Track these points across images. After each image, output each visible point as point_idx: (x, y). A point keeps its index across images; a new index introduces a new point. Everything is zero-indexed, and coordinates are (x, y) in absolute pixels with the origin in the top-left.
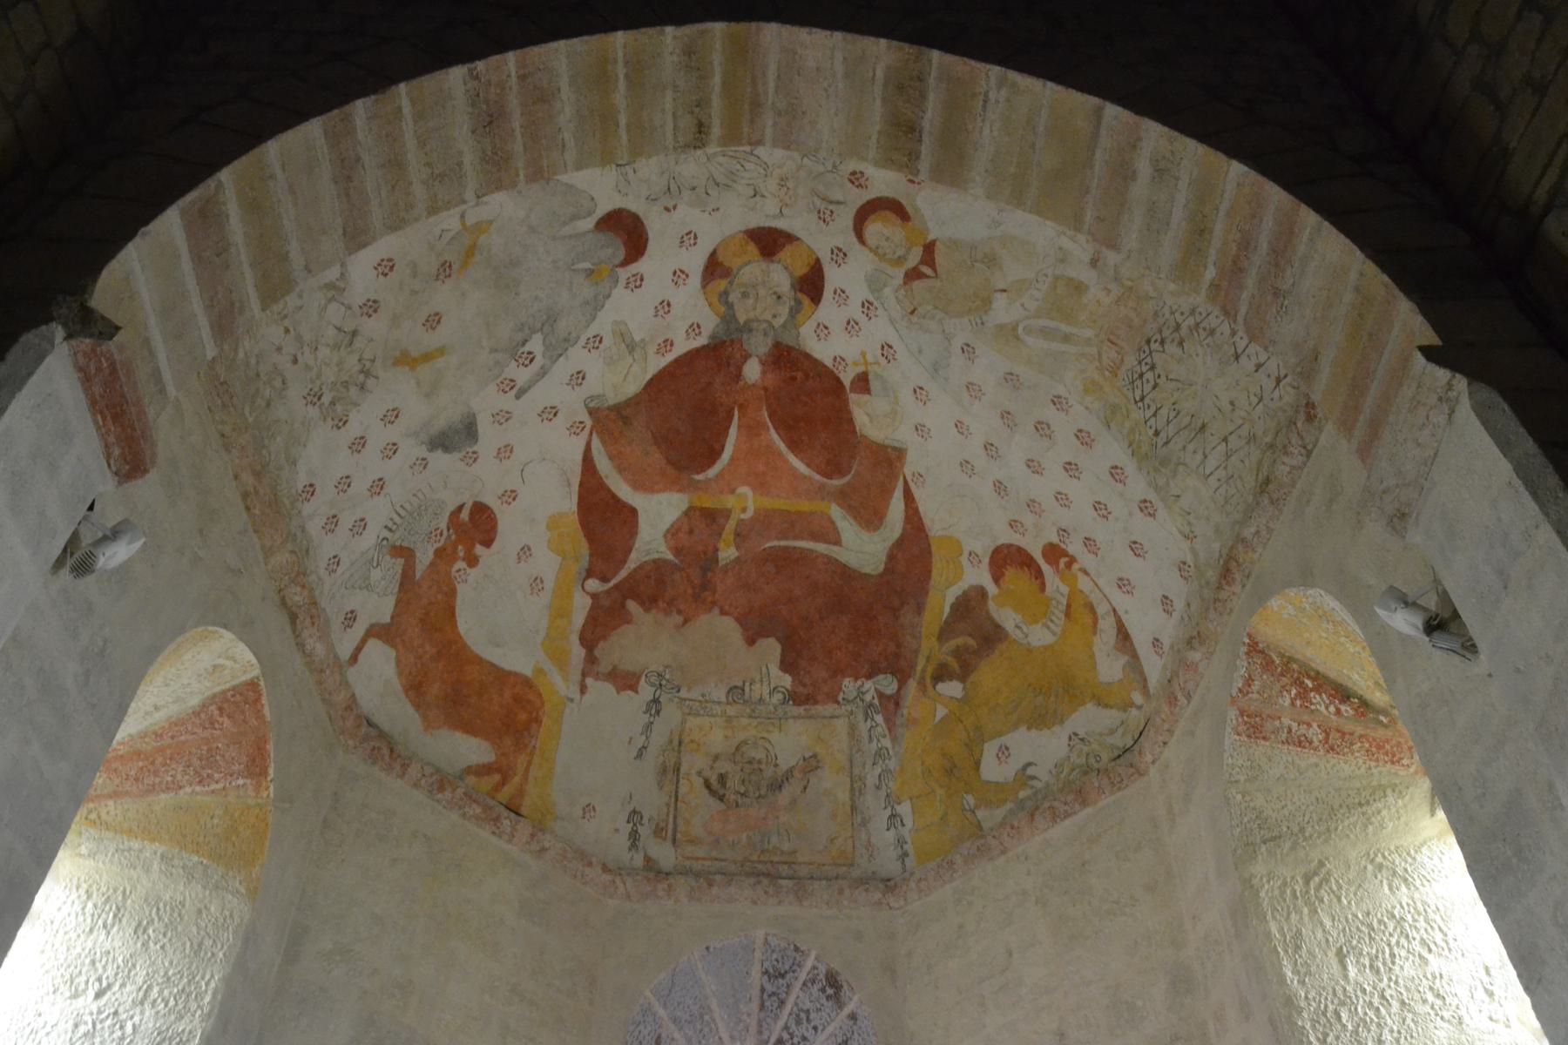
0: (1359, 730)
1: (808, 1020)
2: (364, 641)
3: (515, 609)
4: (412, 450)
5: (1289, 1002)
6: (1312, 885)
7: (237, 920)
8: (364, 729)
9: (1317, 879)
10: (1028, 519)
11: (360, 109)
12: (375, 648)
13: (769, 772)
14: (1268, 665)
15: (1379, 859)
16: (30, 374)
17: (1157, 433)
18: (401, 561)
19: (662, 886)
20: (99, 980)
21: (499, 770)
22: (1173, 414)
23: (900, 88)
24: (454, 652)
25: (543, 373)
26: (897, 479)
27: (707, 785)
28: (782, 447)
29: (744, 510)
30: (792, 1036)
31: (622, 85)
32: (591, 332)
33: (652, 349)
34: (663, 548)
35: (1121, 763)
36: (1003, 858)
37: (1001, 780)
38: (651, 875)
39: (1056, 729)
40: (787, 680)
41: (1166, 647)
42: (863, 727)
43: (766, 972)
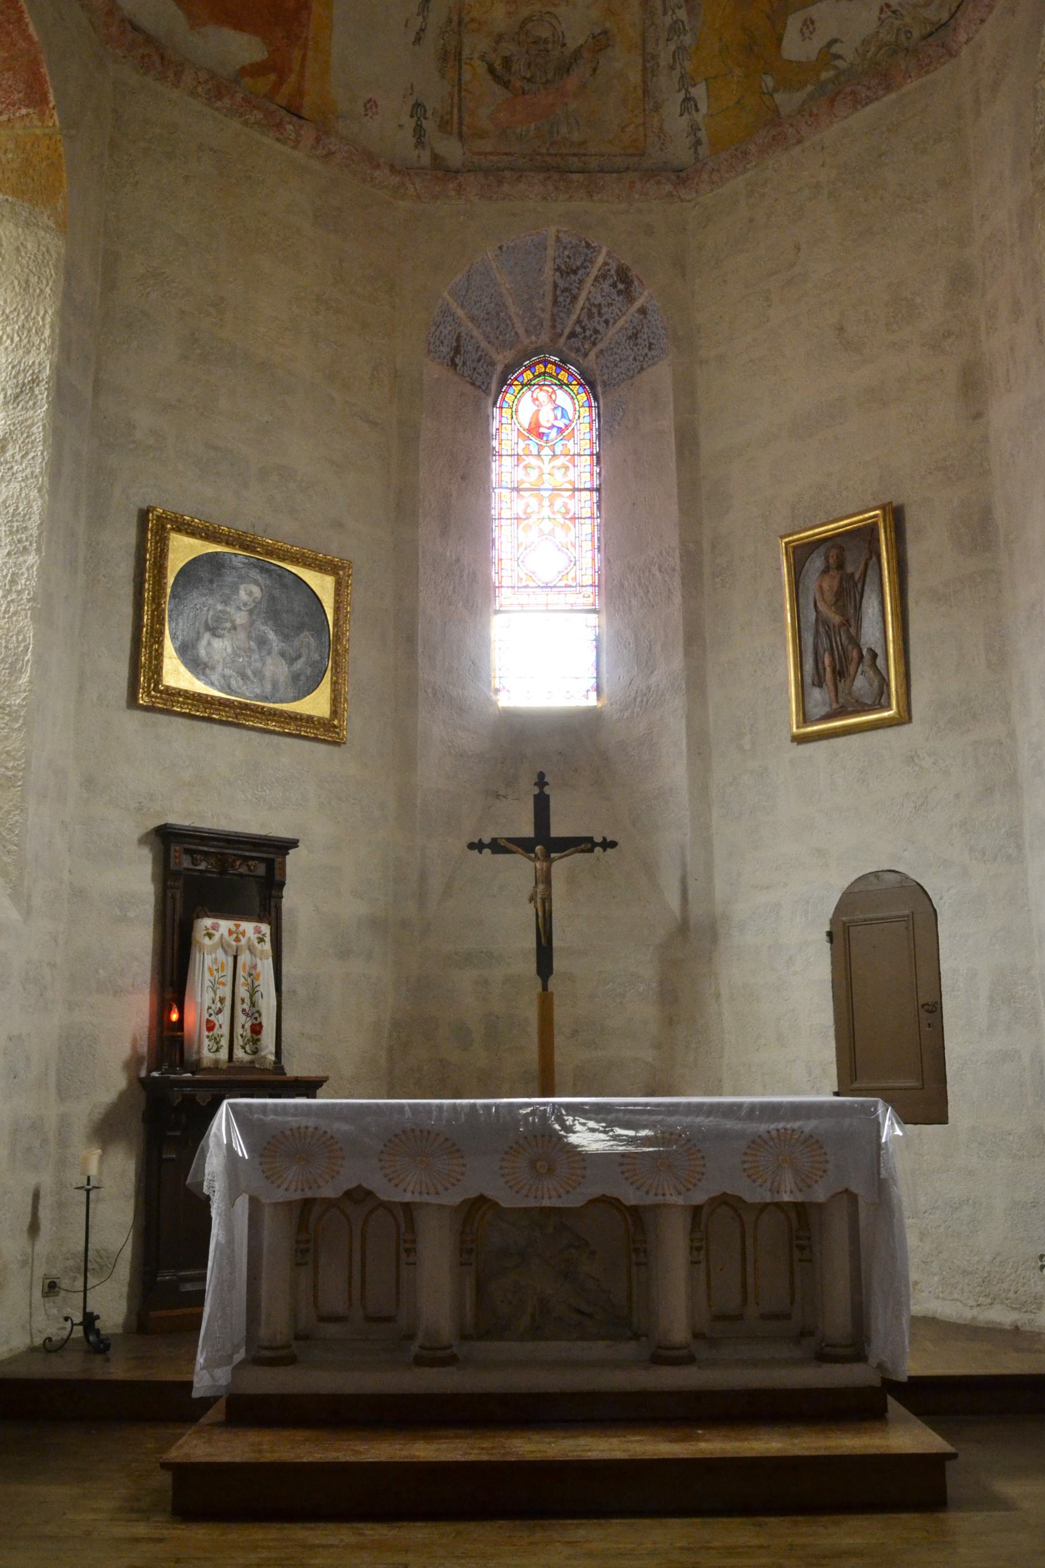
1: (599, 313)
7: (55, 256)
27: (491, 70)
30: (584, 329)
36: (798, 149)
38: (440, 174)
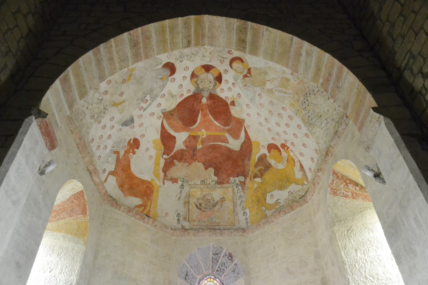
0: (361, 193)
2: (108, 176)
3: (146, 164)
4: (117, 127)
5: (343, 262)
6: (349, 232)
7: (82, 251)
8: (110, 198)
9: (350, 231)
10: (277, 137)
11: (102, 47)
12: (111, 177)
13: (212, 202)
14: (338, 177)
15: (366, 226)
16: (28, 130)
17: (309, 117)
18: (116, 155)
19: (186, 233)
20: (50, 268)
21: (144, 206)
22: (313, 112)
23: (240, 31)
24: (130, 176)
25: (150, 104)
26: (242, 127)
27: (197, 206)
28: (212, 119)
29: (203, 135)
31: (168, 33)
32: (162, 93)
33: (178, 97)
34: (183, 146)
35: (300, 200)
36: (272, 223)
37: (271, 203)
38: (183, 230)
39: (285, 190)
40: (216, 178)
41: (312, 170)
42: (236, 190)
43: (213, 254)
